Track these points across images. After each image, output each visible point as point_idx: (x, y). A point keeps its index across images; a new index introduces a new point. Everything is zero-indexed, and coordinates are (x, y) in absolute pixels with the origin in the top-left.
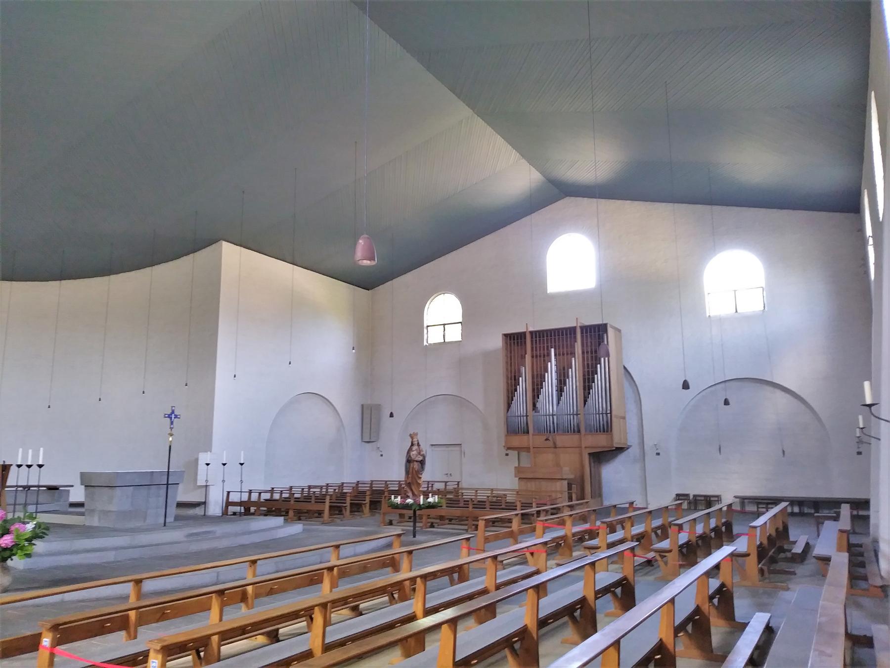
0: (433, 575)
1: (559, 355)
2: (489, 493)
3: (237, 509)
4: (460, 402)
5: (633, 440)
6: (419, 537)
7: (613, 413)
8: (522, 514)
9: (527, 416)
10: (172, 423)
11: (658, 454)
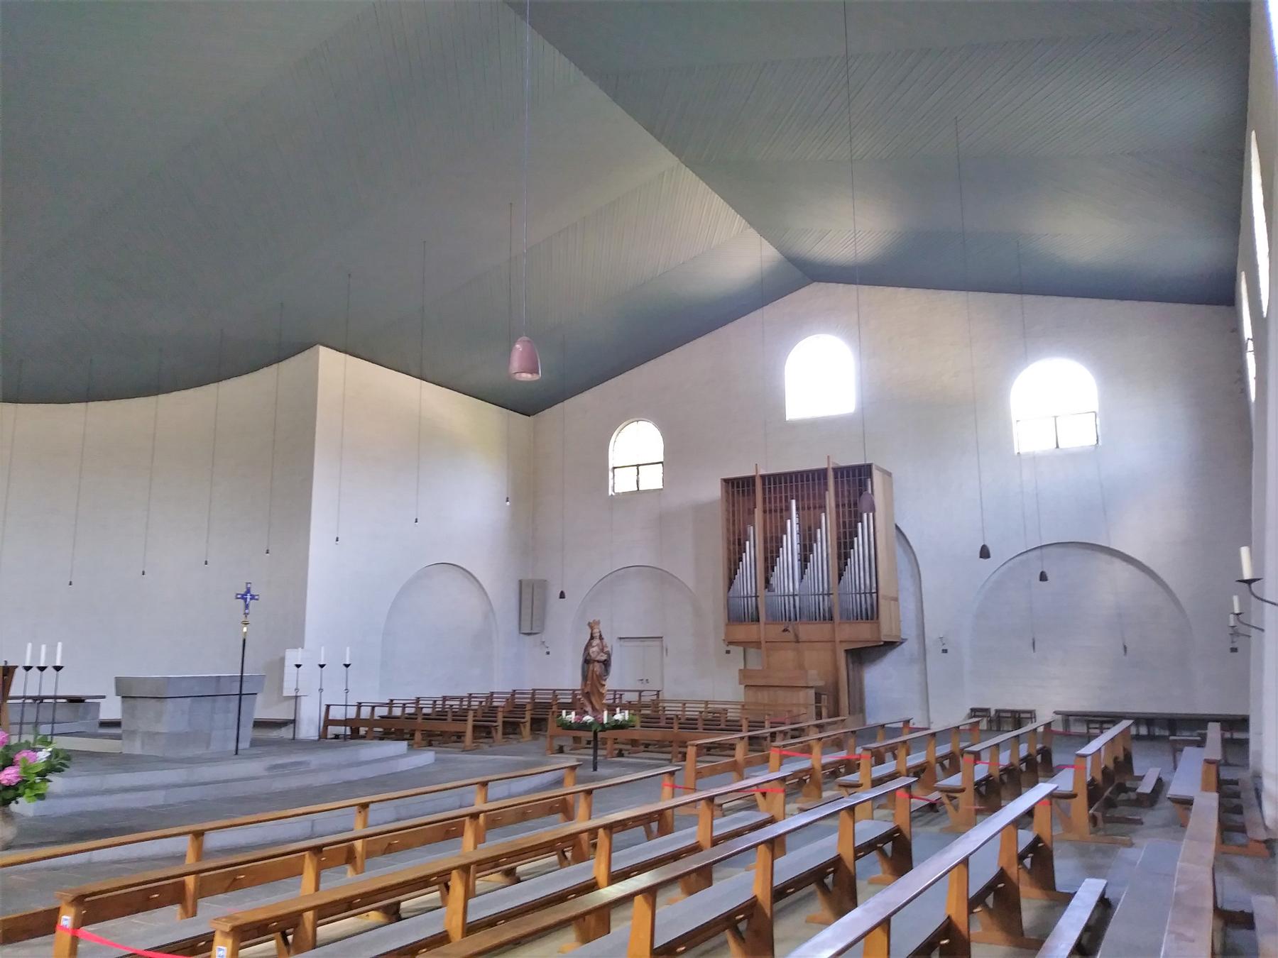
0: (622, 825)
1: (803, 508)
2: (702, 707)
3: (340, 730)
4: (660, 577)
5: (908, 631)
6: (601, 771)
7: (881, 592)
8: (750, 738)
9: (756, 597)
10: (247, 607)
11: (945, 651)
